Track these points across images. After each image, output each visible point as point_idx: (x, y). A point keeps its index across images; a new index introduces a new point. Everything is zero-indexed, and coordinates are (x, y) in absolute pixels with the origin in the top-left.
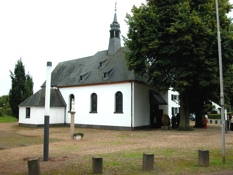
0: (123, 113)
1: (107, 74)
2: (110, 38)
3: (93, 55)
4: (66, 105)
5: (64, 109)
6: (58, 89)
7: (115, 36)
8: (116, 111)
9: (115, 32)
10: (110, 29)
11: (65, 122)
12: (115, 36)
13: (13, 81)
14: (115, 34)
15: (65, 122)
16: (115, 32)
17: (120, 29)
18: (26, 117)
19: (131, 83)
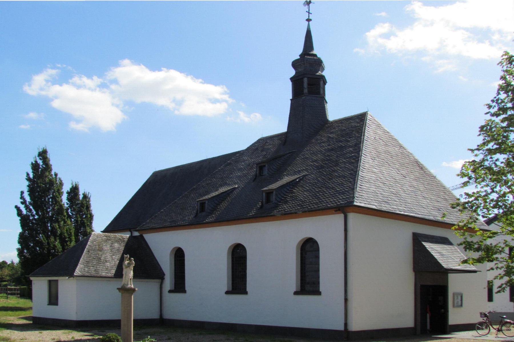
0: (318, 293)
1: (274, 192)
2: (291, 98)
3: (20, 230)
4: (164, 275)
5: (160, 284)
6: (141, 236)
7: (306, 91)
8: (233, 289)
9: (306, 80)
10: (292, 72)
11: (346, 325)
12: (306, 91)
13: (24, 221)
14: (305, 85)
15: (346, 325)
16: (306, 80)
17: (324, 74)
18: (481, 313)
19: (342, 216)
